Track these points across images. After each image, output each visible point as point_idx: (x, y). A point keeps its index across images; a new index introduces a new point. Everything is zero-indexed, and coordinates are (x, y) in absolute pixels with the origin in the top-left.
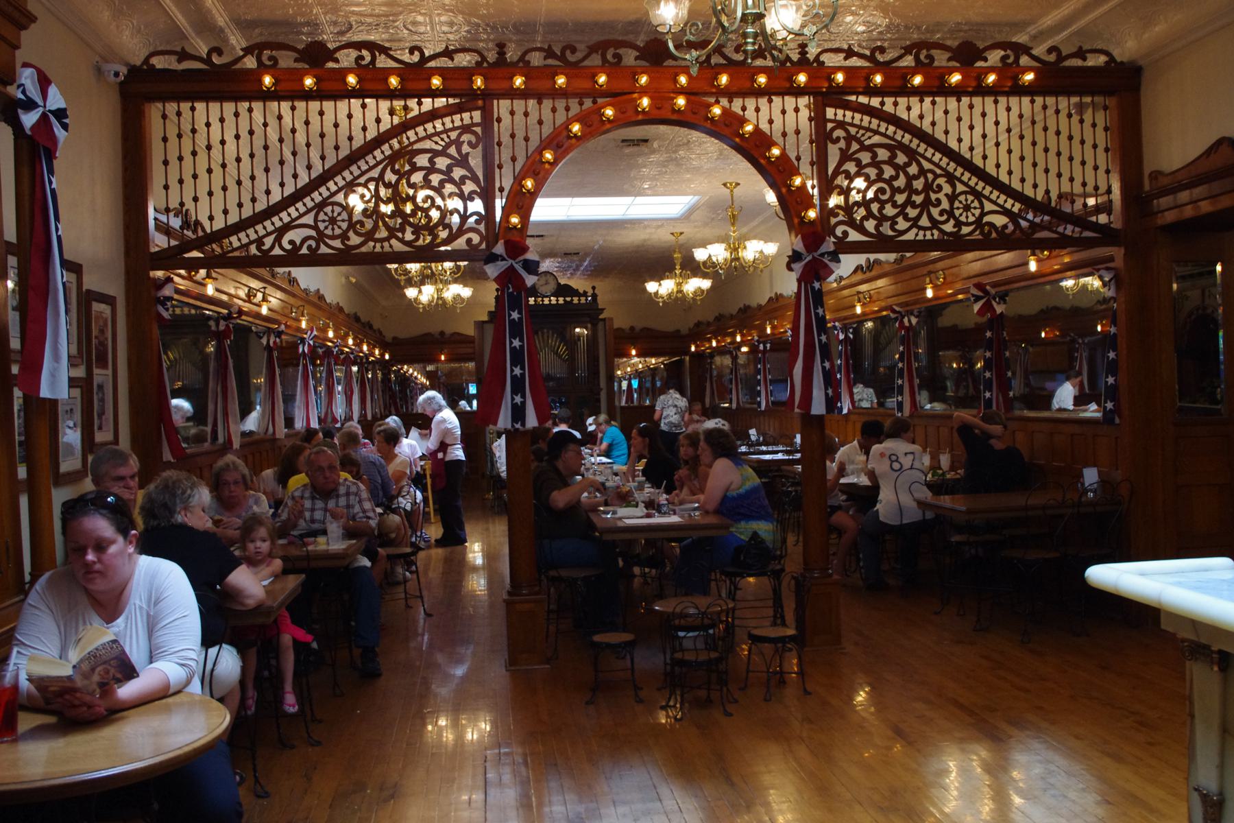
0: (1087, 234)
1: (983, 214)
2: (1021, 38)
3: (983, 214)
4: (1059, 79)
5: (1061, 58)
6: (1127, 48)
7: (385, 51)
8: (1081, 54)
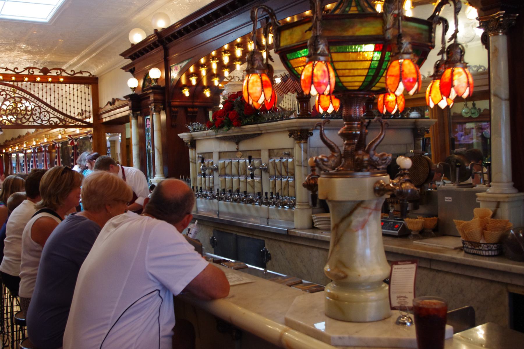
0: (84, 124)
1: (50, 118)
2: (64, 68)
3: (50, 118)
4: (72, 80)
5: (75, 74)
6: (94, 71)
7: (64, 71)
8: (81, 72)
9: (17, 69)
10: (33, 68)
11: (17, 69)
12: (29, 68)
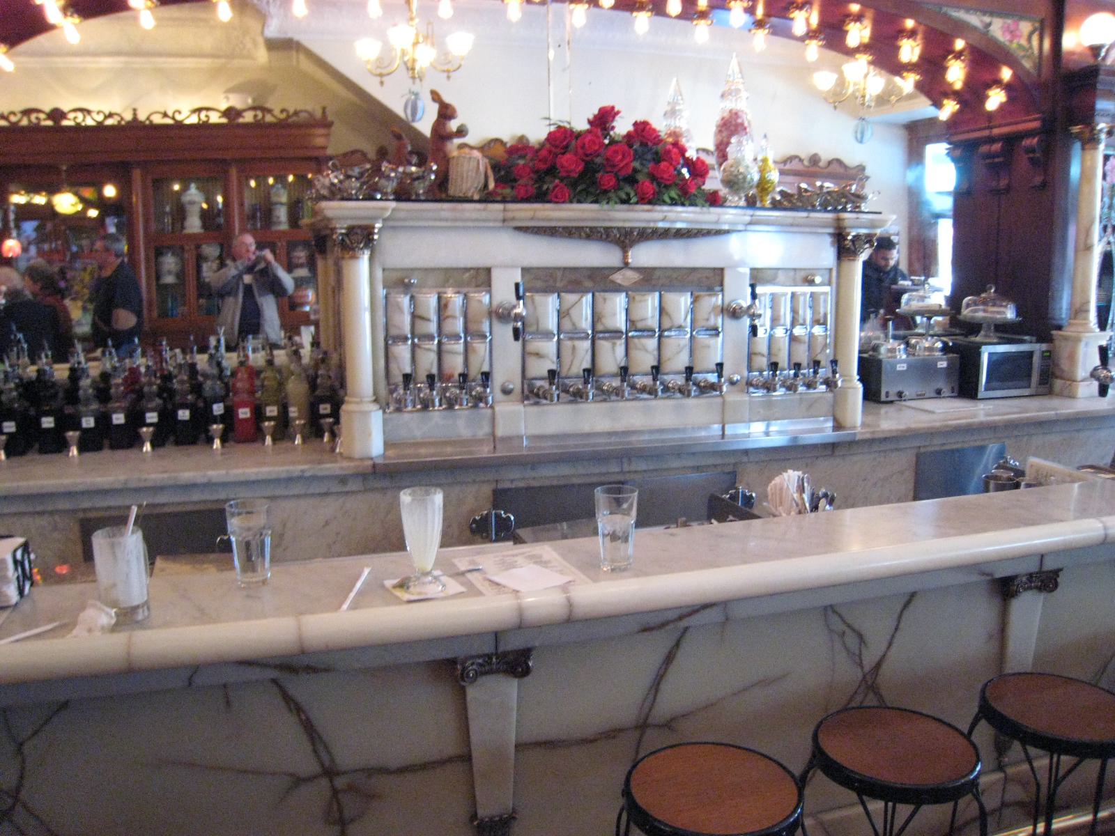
9: (180, 112)
10: (208, 109)
11: (180, 112)
12: (199, 110)
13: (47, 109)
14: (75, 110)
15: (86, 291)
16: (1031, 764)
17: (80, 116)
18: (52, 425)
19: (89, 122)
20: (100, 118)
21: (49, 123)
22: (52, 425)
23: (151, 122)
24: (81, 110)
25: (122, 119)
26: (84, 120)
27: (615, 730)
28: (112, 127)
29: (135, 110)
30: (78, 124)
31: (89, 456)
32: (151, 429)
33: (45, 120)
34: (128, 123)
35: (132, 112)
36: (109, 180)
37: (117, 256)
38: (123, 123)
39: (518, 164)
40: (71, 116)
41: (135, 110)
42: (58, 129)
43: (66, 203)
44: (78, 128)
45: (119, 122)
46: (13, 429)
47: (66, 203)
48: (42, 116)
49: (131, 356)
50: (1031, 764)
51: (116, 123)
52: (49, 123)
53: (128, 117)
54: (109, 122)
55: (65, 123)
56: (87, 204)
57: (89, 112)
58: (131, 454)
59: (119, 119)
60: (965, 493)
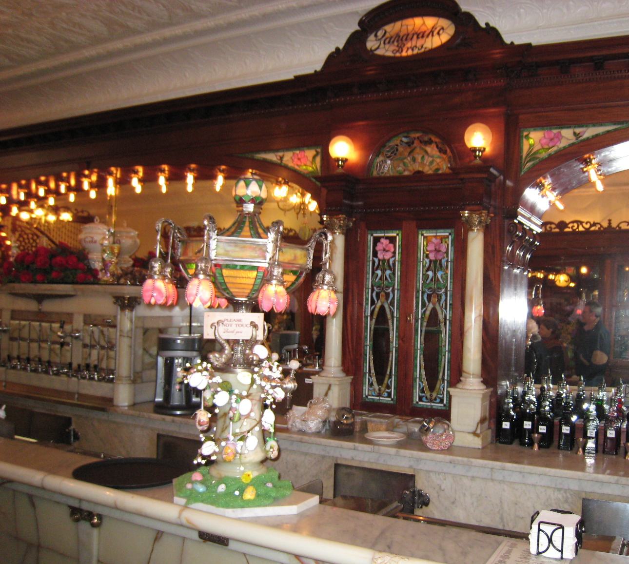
13: (557, 221)
14: (573, 222)
15: (569, 337)
16: (190, 326)
17: (576, 225)
18: (525, 422)
19: (581, 229)
20: (588, 226)
21: (557, 230)
22: (525, 422)
23: (620, 228)
24: (577, 222)
25: (601, 226)
26: (578, 228)
27: (378, 507)
28: (594, 231)
29: (610, 221)
30: (574, 230)
31: (543, 450)
32: (540, 436)
33: (554, 228)
34: (605, 229)
35: (607, 222)
36: (585, 264)
37: (597, 316)
38: (602, 229)
39: (67, 369)
40: (570, 225)
41: (610, 221)
42: (562, 234)
43: (562, 280)
44: (574, 232)
45: (599, 228)
46: (545, 431)
47: (562, 280)
48: (553, 226)
49: (535, 383)
50: (190, 326)
51: (597, 229)
52: (557, 230)
53: (605, 224)
54: (593, 229)
55: (567, 230)
56: (572, 279)
57: (581, 223)
58: (526, 449)
59: (599, 226)
60: (608, 552)
